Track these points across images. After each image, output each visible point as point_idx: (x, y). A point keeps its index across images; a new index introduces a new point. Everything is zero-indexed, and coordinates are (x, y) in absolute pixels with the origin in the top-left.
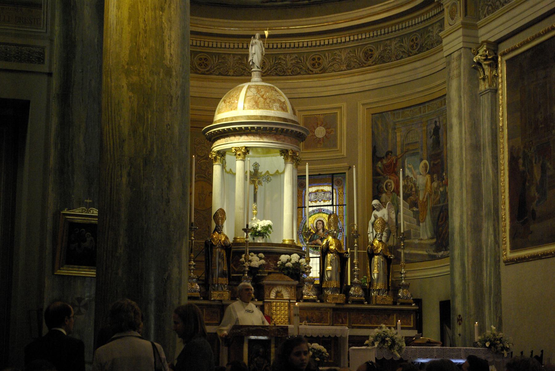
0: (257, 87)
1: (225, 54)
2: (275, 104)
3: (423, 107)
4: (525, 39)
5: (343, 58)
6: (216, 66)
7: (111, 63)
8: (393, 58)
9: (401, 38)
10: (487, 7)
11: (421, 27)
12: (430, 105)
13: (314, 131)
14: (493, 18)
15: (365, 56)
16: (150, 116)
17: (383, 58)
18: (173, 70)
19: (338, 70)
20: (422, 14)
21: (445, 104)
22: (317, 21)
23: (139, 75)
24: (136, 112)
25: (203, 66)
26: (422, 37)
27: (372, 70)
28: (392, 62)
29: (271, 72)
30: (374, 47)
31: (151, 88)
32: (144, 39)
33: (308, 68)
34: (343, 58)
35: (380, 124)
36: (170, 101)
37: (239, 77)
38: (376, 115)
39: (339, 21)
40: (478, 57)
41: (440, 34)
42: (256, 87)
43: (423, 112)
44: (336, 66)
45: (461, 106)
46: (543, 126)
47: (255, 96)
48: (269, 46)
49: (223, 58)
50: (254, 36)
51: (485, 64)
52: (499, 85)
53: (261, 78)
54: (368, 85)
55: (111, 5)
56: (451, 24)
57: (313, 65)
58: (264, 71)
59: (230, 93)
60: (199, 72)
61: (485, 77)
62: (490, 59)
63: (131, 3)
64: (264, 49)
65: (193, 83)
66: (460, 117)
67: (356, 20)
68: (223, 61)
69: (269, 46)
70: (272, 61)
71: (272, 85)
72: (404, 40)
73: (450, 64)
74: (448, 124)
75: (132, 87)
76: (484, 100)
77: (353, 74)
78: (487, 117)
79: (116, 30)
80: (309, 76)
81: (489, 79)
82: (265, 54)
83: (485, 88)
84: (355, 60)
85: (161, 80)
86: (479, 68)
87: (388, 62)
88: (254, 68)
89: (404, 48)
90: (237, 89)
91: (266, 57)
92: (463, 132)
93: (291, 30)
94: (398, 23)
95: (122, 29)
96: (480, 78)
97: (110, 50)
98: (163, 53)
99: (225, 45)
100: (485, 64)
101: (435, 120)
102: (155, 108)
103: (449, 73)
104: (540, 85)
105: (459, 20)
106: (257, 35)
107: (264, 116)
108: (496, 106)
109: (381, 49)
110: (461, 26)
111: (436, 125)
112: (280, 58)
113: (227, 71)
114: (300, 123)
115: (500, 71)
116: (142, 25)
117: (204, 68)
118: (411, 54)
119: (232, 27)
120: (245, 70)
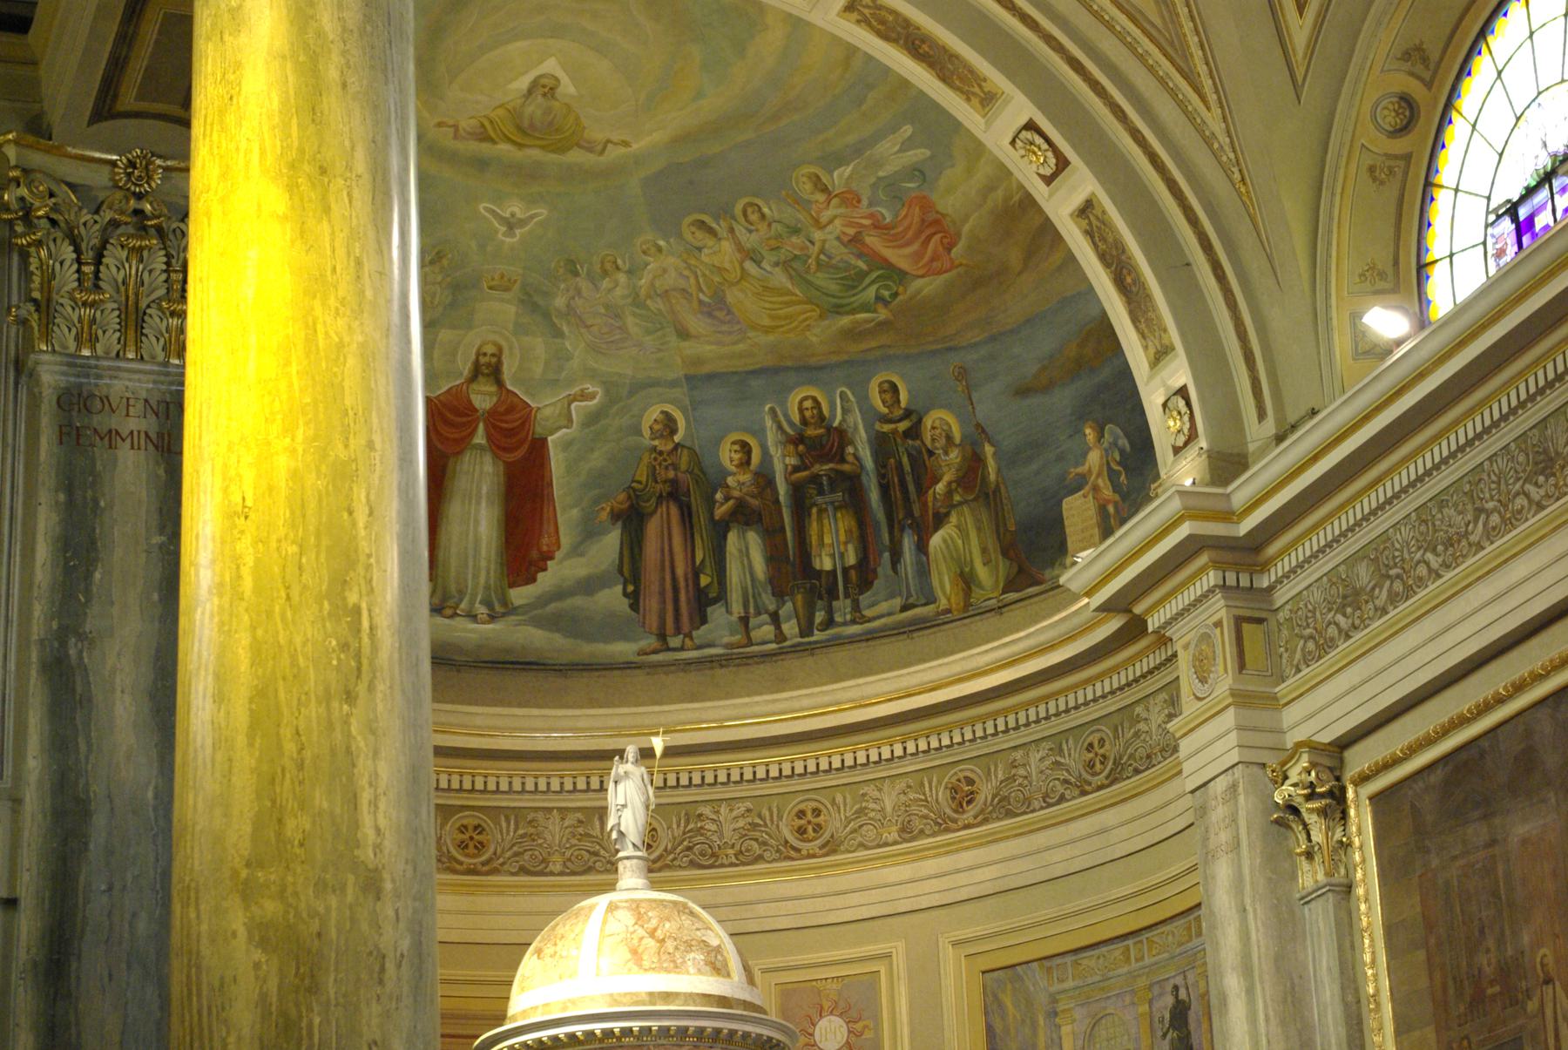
0: (636, 907)
1: (536, 809)
2: (692, 955)
3: (1135, 944)
4: (1421, 733)
5: (889, 809)
6: (511, 848)
7: (197, 863)
8: (1036, 803)
9: (1057, 742)
10: (1302, 642)
11: (1113, 708)
12: (1155, 939)
13: (810, 1031)
14: (1320, 674)
15: (953, 798)
16: (317, 1020)
17: (1004, 803)
18: (386, 875)
19: (875, 843)
20: (1115, 669)
21: (1199, 934)
22: (806, 702)
23: (281, 895)
24: (274, 1008)
25: (471, 850)
26: (1116, 737)
27: (976, 838)
28: (1035, 815)
29: (675, 859)
30: (979, 771)
31: (319, 935)
32: (298, 789)
33: (787, 842)
34: (889, 809)
35: (1008, 1001)
36: (377, 968)
37: (578, 878)
38: (996, 974)
39: (869, 698)
40: (1287, 788)
41: (1169, 726)
42: (634, 906)
43: (1137, 960)
44: (869, 833)
45: (1249, 939)
46: (1497, 989)
47: (632, 933)
48: (665, 780)
49: (530, 822)
50: (621, 753)
51: (1311, 811)
52: (1355, 870)
53: (648, 878)
54: (966, 884)
55: (197, 691)
56: (1199, 695)
57: (801, 831)
58: (652, 857)
59: (553, 929)
60: (458, 867)
61: (1313, 847)
62: (1322, 796)
63: (256, 682)
64: (651, 791)
65: (444, 901)
66: (1247, 970)
67: (920, 693)
68: (532, 830)
69: (665, 780)
70: (678, 826)
71: (681, 899)
72: (1065, 747)
73: (1205, 813)
74: (1213, 992)
75: (263, 935)
76: (1314, 917)
77: (920, 855)
78: (1329, 969)
79: (213, 766)
80: (790, 863)
81: (1326, 853)
82: (658, 805)
83: (1316, 881)
84: (925, 811)
85: (351, 907)
86: (1293, 821)
87: (1025, 813)
88: (623, 849)
89: (1067, 770)
90: (577, 915)
91: (658, 813)
92: (1261, 1016)
93: (728, 730)
94: (1045, 699)
95: (230, 760)
96: (1298, 851)
97: (194, 825)
98: (355, 824)
99: (536, 784)
100: (1311, 811)
101: (1172, 982)
102: (332, 992)
103: (1206, 839)
104: (1477, 866)
105: (1224, 682)
106: (631, 751)
107: (660, 993)
108: (1351, 935)
109: (1001, 776)
110: (1230, 700)
111: (1177, 996)
112: (700, 815)
113: (542, 862)
114: (767, 1008)
115: (1354, 829)
116: (290, 747)
117: (474, 856)
118: (1088, 788)
119: (556, 730)
120: (596, 854)
